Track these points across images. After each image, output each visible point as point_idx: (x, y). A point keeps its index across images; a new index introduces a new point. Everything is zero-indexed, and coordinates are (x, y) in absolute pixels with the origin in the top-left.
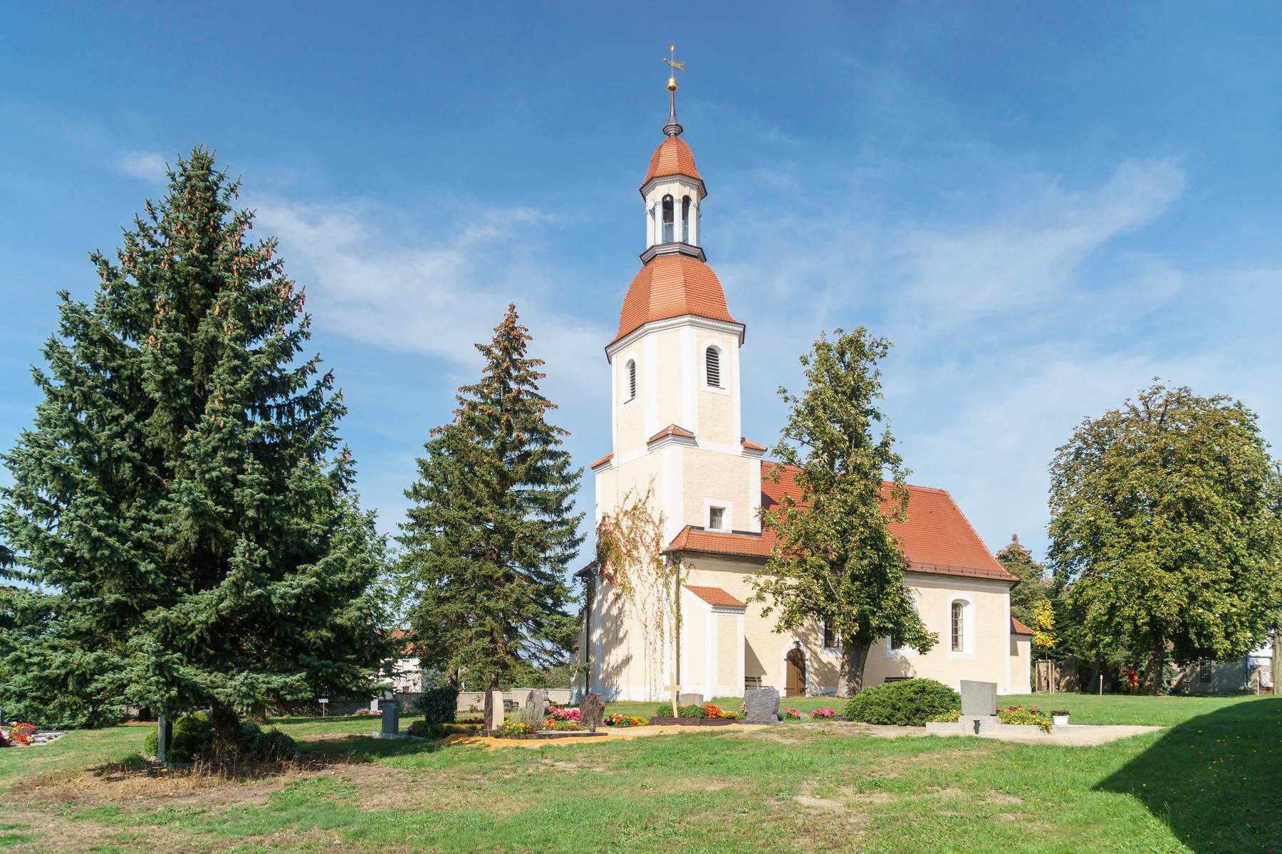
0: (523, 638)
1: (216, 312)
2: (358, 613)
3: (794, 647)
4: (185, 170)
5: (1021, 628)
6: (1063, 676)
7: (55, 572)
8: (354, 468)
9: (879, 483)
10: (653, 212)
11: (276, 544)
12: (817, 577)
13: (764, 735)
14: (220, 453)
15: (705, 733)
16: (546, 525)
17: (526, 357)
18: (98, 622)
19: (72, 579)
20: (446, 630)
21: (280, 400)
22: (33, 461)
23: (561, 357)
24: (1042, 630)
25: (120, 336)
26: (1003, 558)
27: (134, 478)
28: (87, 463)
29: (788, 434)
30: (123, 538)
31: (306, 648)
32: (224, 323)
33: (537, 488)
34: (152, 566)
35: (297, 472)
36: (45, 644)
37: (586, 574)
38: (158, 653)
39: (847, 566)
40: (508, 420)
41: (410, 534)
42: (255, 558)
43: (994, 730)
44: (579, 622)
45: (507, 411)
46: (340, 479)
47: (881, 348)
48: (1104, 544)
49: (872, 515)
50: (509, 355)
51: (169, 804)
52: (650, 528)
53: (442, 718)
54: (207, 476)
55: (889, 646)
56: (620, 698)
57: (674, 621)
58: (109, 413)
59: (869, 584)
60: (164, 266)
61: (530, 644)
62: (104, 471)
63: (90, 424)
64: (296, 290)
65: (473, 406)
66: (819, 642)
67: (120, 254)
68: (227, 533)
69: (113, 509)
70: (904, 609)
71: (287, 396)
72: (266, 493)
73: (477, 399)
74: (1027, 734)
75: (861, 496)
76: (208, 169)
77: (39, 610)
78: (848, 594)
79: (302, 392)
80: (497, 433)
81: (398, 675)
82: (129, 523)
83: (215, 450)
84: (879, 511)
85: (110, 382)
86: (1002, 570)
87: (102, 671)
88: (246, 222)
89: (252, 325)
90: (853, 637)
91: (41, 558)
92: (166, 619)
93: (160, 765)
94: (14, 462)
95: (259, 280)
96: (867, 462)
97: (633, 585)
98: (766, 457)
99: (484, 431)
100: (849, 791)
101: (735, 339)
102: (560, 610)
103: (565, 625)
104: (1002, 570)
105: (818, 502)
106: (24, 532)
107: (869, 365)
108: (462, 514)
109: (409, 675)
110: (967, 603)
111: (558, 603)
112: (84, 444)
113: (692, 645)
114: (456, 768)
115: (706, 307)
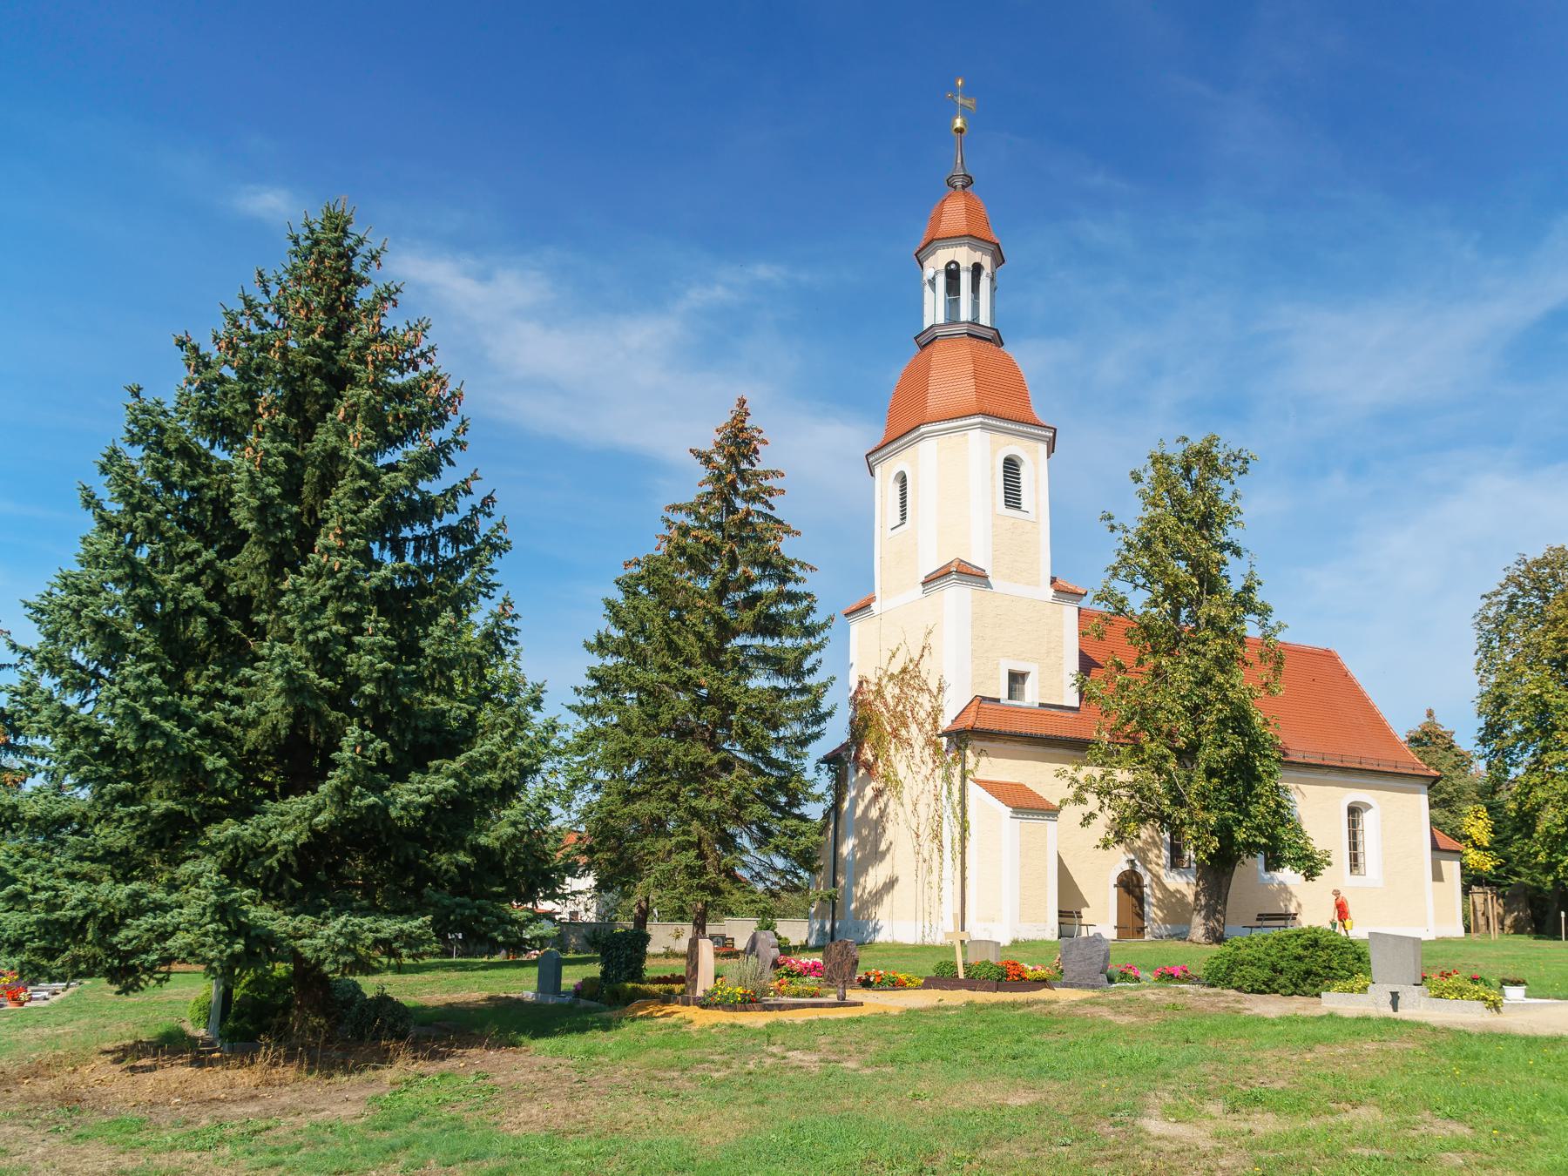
0: (743, 851)
1: (340, 417)
2: (510, 830)
3: (1127, 867)
4: (312, 231)
5: (1446, 842)
6: (1508, 911)
7: (84, 769)
8: (517, 624)
9: (1242, 641)
10: (932, 282)
11: (402, 733)
12: (1159, 770)
13: (1089, 1009)
14: (331, 606)
15: (1003, 1005)
16: (779, 693)
17: (759, 467)
18: (140, 838)
19: (108, 779)
20: (633, 839)
21: (420, 530)
22: (66, 613)
23: (805, 454)
24: (1475, 846)
25: (206, 445)
26: (1415, 741)
27: (207, 637)
28: (144, 613)
29: (1115, 575)
30: (185, 721)
31: (436, 877)
32: (350, 432)
33: (769, 643)
34: (223, 762)
35: (437, 632)
36: (59, 871)
37: (834, 760)
38: (220, 890)
39: (1201, 756)
40: (732, 551)
41: (591, 702)
42: (369, 753)
43: (1420, 1008)
44: (822, 831)
45: (731, 537)
46: (496, 640)
47: (1240, 462)
48: (1555, 728)
49: (1233, 686)
50: (736, 464)
51: (219, 1113)
52: (925, 699)
53: (624, 974)
54: (311, 637)
55: (1261, 867)
56: (880, 938)
57: (958, 830)
58: (180, 549)
59: (1232, 781)
60: (274, 355)
61: (751, 857)
62: (167, 627)
63: (153, 562)
64: (452, 386)
65: (685, 531)
66: (1163, 861)
67: (216, 338)
68: (334, 715)
69: (175, 681)
70: (1282, 817)
71: (430, 524)
72: (392, 662)
73: (690, 521)
74: (1465, 1014)
75: (1217, 660)
76: (344, 230)
77: (55, 821)
78: (1202, 795)
79: (451, 520)
80: (716, 567)
81: (564, 897)
82: (196, 700)
83: (325, 601)
84: (1243, 681)
85: (187, 505)
86: (1412, 759)
87: (139, 912)
88: (389, 298)
89: (387, 432)
90: (1210, 856)
91: (65, 749)
92: (236, 838)
93: (211, 1044)
94: (43, 612)
95: (402, 373)
96: (1225, 615)
97: (901, 777)
98: (1085, 603)
99: (698, 564)
100: (1214, 1108)
101: (1043, 447)
102: (796, 811)
103: (803, 834)
104: (1412, 759)
105: (1159, 666)
106: (45, 713)
107: (1224, 484)
108: (664, 677)
109: (579, 898)
110: (1368, 807)
111: (794, 801)
112: (142, 591)
113: (982, 868)
114: (643, 1059)
115: (1004, 406)
